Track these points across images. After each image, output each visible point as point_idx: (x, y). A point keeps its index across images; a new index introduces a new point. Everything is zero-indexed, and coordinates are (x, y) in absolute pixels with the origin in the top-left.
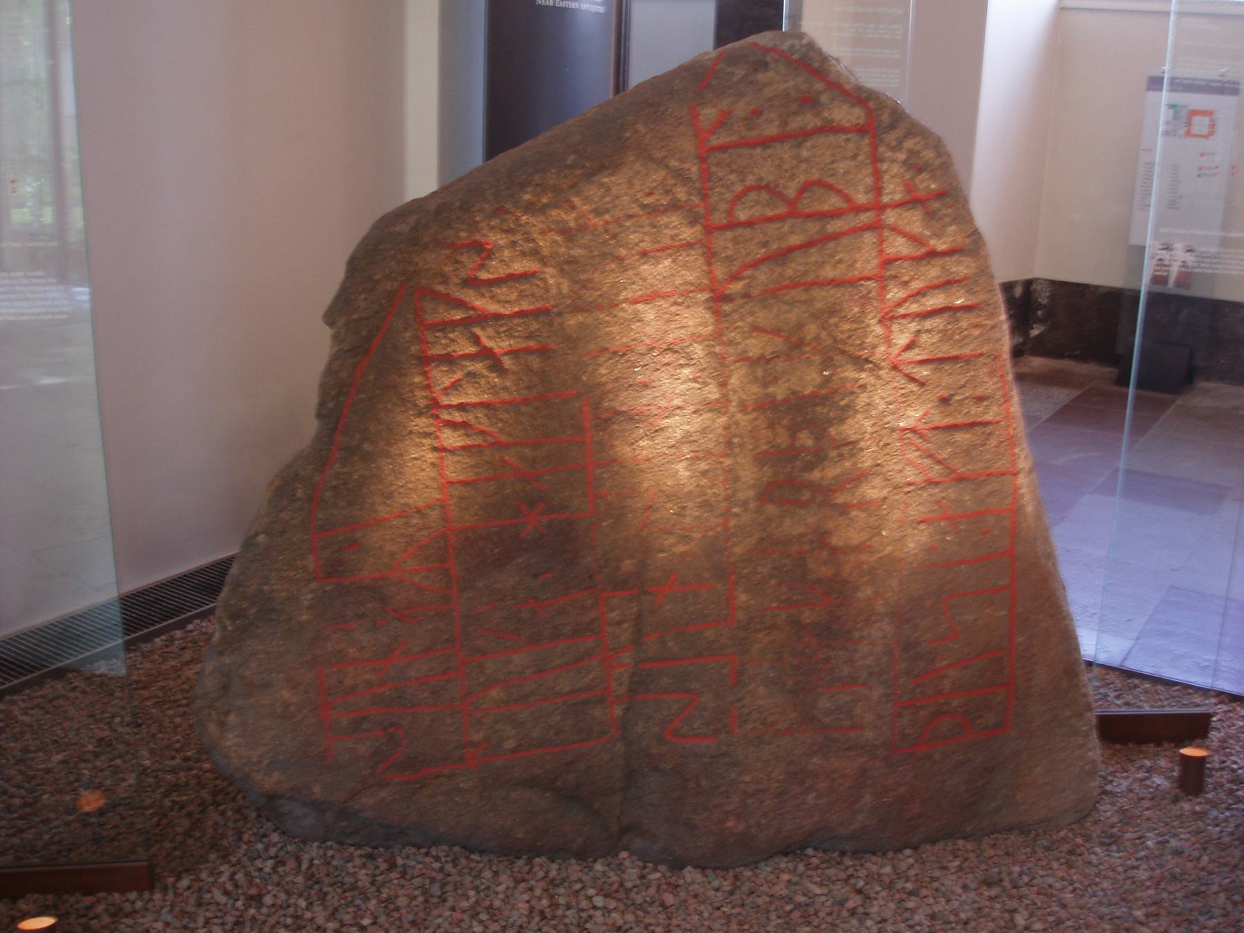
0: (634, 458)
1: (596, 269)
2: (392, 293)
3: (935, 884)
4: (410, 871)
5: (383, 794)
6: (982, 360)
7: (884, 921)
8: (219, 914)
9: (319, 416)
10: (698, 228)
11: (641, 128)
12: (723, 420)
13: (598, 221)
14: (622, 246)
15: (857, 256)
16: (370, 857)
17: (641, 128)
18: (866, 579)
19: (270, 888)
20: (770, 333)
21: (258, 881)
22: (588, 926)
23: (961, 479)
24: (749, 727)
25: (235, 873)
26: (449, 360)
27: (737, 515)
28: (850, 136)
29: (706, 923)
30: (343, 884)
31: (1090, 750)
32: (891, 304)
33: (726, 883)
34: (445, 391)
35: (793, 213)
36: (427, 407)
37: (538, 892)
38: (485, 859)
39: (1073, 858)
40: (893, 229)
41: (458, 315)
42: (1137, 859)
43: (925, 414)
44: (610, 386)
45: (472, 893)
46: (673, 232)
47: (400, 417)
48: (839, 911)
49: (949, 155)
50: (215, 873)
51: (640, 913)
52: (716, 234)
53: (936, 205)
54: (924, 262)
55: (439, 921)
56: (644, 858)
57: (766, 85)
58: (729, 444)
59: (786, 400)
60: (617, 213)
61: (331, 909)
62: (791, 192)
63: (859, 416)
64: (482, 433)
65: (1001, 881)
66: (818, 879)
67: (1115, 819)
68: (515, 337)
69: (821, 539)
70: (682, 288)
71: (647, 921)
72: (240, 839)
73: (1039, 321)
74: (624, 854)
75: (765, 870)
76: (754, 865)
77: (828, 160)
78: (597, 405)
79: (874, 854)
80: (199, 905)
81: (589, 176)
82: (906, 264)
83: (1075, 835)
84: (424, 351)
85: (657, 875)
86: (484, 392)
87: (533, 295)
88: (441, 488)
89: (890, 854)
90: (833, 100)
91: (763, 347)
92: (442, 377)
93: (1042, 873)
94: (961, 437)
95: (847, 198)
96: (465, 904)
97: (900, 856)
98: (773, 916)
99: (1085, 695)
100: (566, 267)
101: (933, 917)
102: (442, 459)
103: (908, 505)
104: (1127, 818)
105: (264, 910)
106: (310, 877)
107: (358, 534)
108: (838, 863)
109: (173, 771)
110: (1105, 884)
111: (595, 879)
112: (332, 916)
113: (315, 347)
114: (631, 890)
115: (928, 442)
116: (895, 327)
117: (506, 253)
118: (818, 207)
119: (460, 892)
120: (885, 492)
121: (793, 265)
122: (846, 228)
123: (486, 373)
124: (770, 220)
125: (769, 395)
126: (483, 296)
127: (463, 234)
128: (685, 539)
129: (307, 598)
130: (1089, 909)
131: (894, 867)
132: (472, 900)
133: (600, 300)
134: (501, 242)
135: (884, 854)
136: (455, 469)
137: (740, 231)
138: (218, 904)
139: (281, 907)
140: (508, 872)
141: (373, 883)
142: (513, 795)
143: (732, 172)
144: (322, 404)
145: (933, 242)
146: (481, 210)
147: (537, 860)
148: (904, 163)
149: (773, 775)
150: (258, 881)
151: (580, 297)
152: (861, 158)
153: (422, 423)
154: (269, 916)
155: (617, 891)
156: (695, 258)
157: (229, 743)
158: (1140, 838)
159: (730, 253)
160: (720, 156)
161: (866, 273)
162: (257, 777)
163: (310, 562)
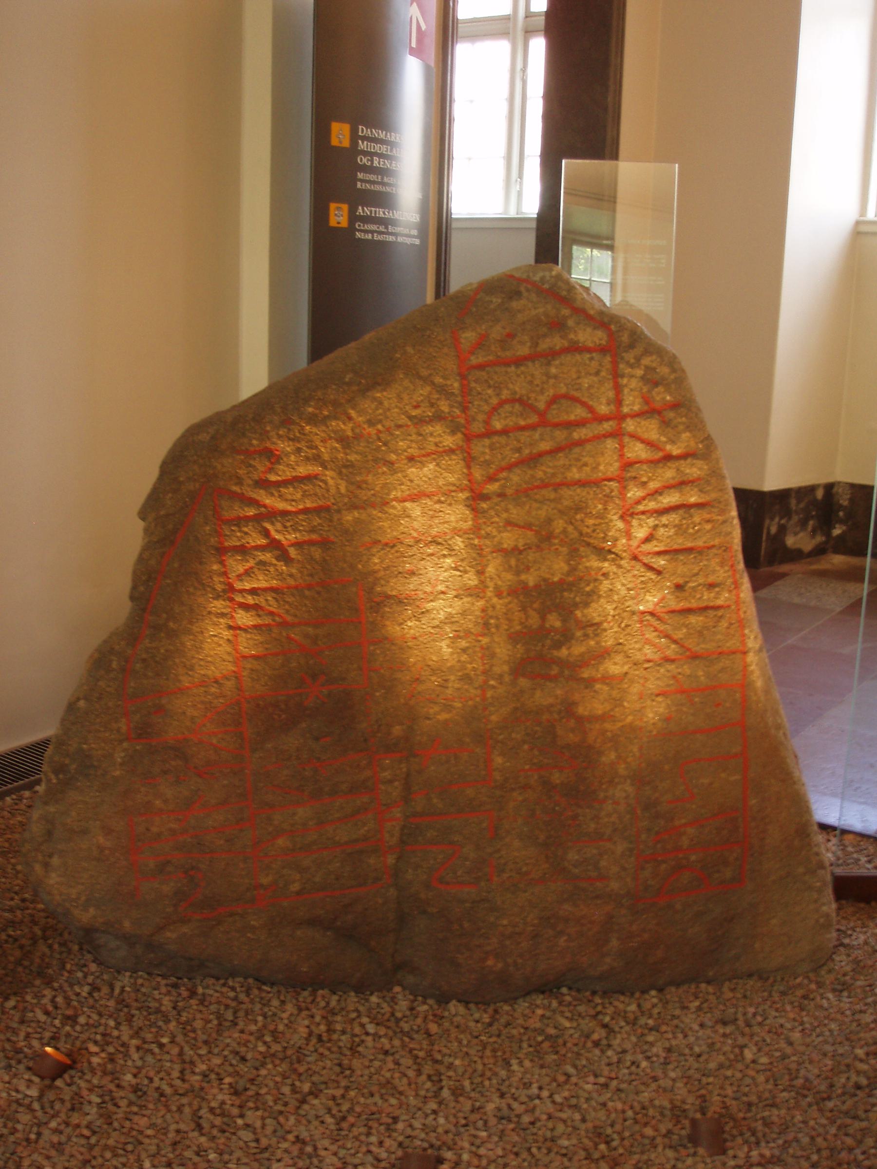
0: (403, 637)
1: (369, 472)
2: (197, 492)
3: (676, 1022)
4: (208, 998)
5: (185, 929)
6: (714, 551)
7: (624, 1051)
8: (39, 1030)
9: (132, 598)
10: (459, 435)
11: (410, 350)
12: (481, 603)
13: (373, 431)
14: (392, 452)
15: (601, 459)
16: (175, 986)
17: (410, 350)
18: (609, 745)
19: (85, 1009)
20: (523, 527)
21: (75, 1003)
22: (360, 1049)
23: (695, 657)
24: (505, 876)
25: (55, 997)
26: (242, 550)
27: (493, 687)
28: (594, 354)
29: (465, 1049)
30: (149, 1007)
31: (824, 904)
32: (630, 502)
33: (485, 1016)
34: (239, 577)
35: (543, 422)
36: (224, 591)
37: (318, 1019)
38: (275, 989)
39: (806, 1002)
40: (633, 436)
41: (251, 512)
42: (866, 1004)
43: (663, 599)
44: (382, 573)
45: (260, 1018)
46: (437, 440)
47: (201, 600)
48: (585, 1042)
49: (683, 371)
50: (38, 996)
51: (406, 1039)
52: (475, 441)
53: (671, 414)
54: (661, 465)
55: (228, 1041)
56: (414, 992)
57: (519, 311)
58: (486, 625)
59: (536, 586)
60: (388, 424)
61: (135, 1028)
62: (541, 406)
63: (602, 600)
64: (271, 613)
65: (736, 1020)
66: (568, 1015)
67: (848, 968)
68: (300, 531)
69: (568, 709)
70: (445, 488)
71: (411, 1046)
72: (64, 968)
73: (841, 522)
74: (397, 989)
75: (522, 1006)
76: (512, 1000)
77: (574, 376)
78: (371, 590)
79: (623, 994)
80: (22, 1022)
81: (364, 391)
82: (645, 467)
83: (811, 981)
84: (221, 543)
85: (425, 1007)
86: (273, 578)
87: (316, 495)
88: (235, 663)
89: (637, 995)
90: (578, 324)
91: (517, 540)
92: (236, 565)
93: (774, 1013)
94: (694, 620)
95: (591, 409)
96: (253, 1028)
97: (647, 996)
98: (525, 1045)
99: (817, 854)
100: (344, 470)
101: (669, 1050)
102: (236, 636)
103: (646, 680)
104: (859, 967)
105: (78, 1028)
106: (120, 1001)
107: (164, 701)
108: (589, 1001)
109: (11, 910)
110: (833, 1026)
111: (370, 1010)
112: (136, 1034)
113: (132, 536)
114: (401, 1019)
115: (665, 623)
116: (635, 522)
117: (293, 458)
118: (565, 417)
119: (250, 1017)
120: (626, 668)
121: (544, 468)
122: (591, 435)
123: (274, 561)
124: (522, 428)
125: (523, 582)
126: (272, 495)
127: (255, 442)
128: (448, 708)
129: (119, 757)
130: (815, 1047)
131: (639, 1006)
132: (260, 1024)
133: (373, 499)
134: (288, 449)
135: (632, 994)
136: (247, 645)
137: (496, 439)
138: (39, 1022)
139: (93, 1025)
140: (294, 1001)
141: (174, 1008)
142: (299, 933)
143: (490, 387)
144: (134, 587)
145: (668, 447)
146: (271, 422)
147: (321, 992)
148: (642, 378)
149: (529, 919)
150: (75, 1003)
151: (356, 497)
152: (603, 374)
153: (219, 605)
154: (81, 1033)
155: (388, 1020)
156: (456, 462)
157: (52, 882)
158: (870, 986)
159: (487, 457)
160: (483, 374)
161: (609, 474)
162: (76, 912)
163: (123, 725)
